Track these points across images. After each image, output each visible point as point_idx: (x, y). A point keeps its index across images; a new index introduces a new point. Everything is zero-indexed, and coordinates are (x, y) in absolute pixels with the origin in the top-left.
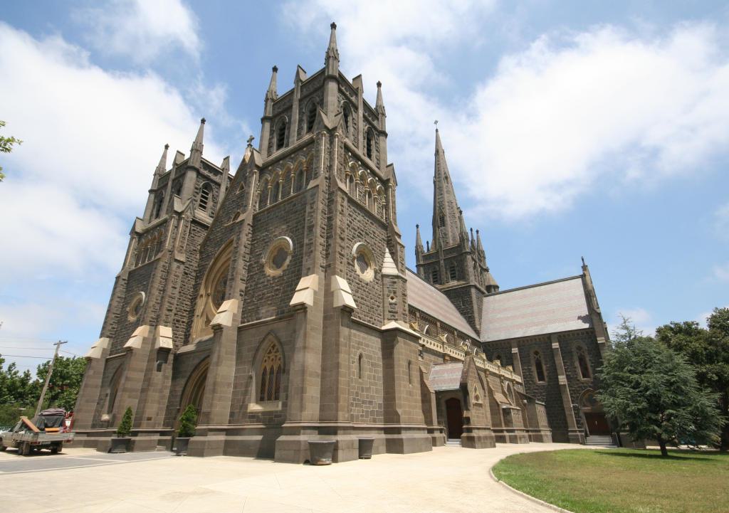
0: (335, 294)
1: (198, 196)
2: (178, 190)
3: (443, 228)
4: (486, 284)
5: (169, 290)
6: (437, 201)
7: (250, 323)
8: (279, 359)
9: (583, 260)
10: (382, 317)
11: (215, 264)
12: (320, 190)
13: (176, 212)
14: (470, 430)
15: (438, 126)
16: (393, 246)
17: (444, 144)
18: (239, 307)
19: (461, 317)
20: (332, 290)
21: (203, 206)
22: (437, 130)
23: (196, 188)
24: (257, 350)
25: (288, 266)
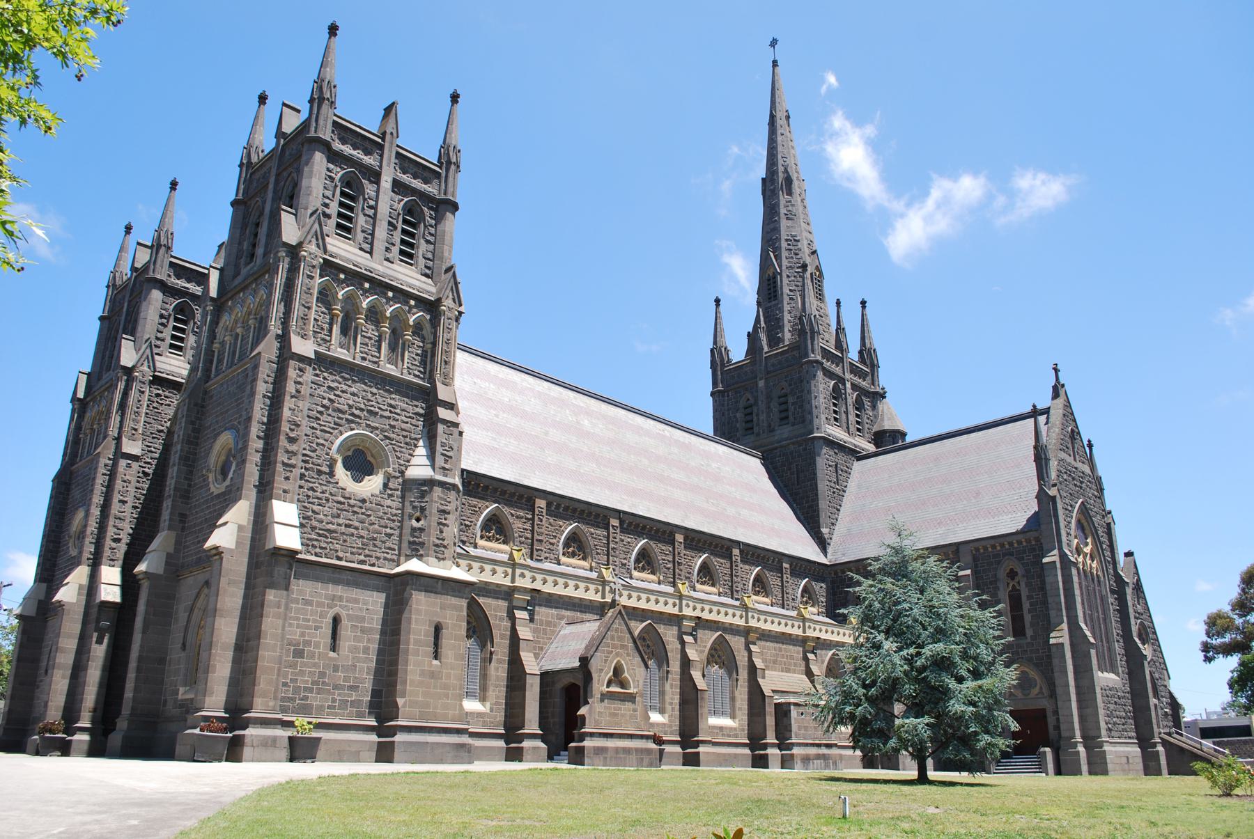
1: (165, 330)
2: (291, 197)
4: (876, 428)
5: (115, 507)
9: (1056, 370)
10: (396, 552)
12: (263, 362)
13: (124, 368)
14: (582, 737)
15: (780, 53)
17: (787, 101)
21: (344, 229)
22: (775, 63)
23: (162, 316)
24: (192, 610)
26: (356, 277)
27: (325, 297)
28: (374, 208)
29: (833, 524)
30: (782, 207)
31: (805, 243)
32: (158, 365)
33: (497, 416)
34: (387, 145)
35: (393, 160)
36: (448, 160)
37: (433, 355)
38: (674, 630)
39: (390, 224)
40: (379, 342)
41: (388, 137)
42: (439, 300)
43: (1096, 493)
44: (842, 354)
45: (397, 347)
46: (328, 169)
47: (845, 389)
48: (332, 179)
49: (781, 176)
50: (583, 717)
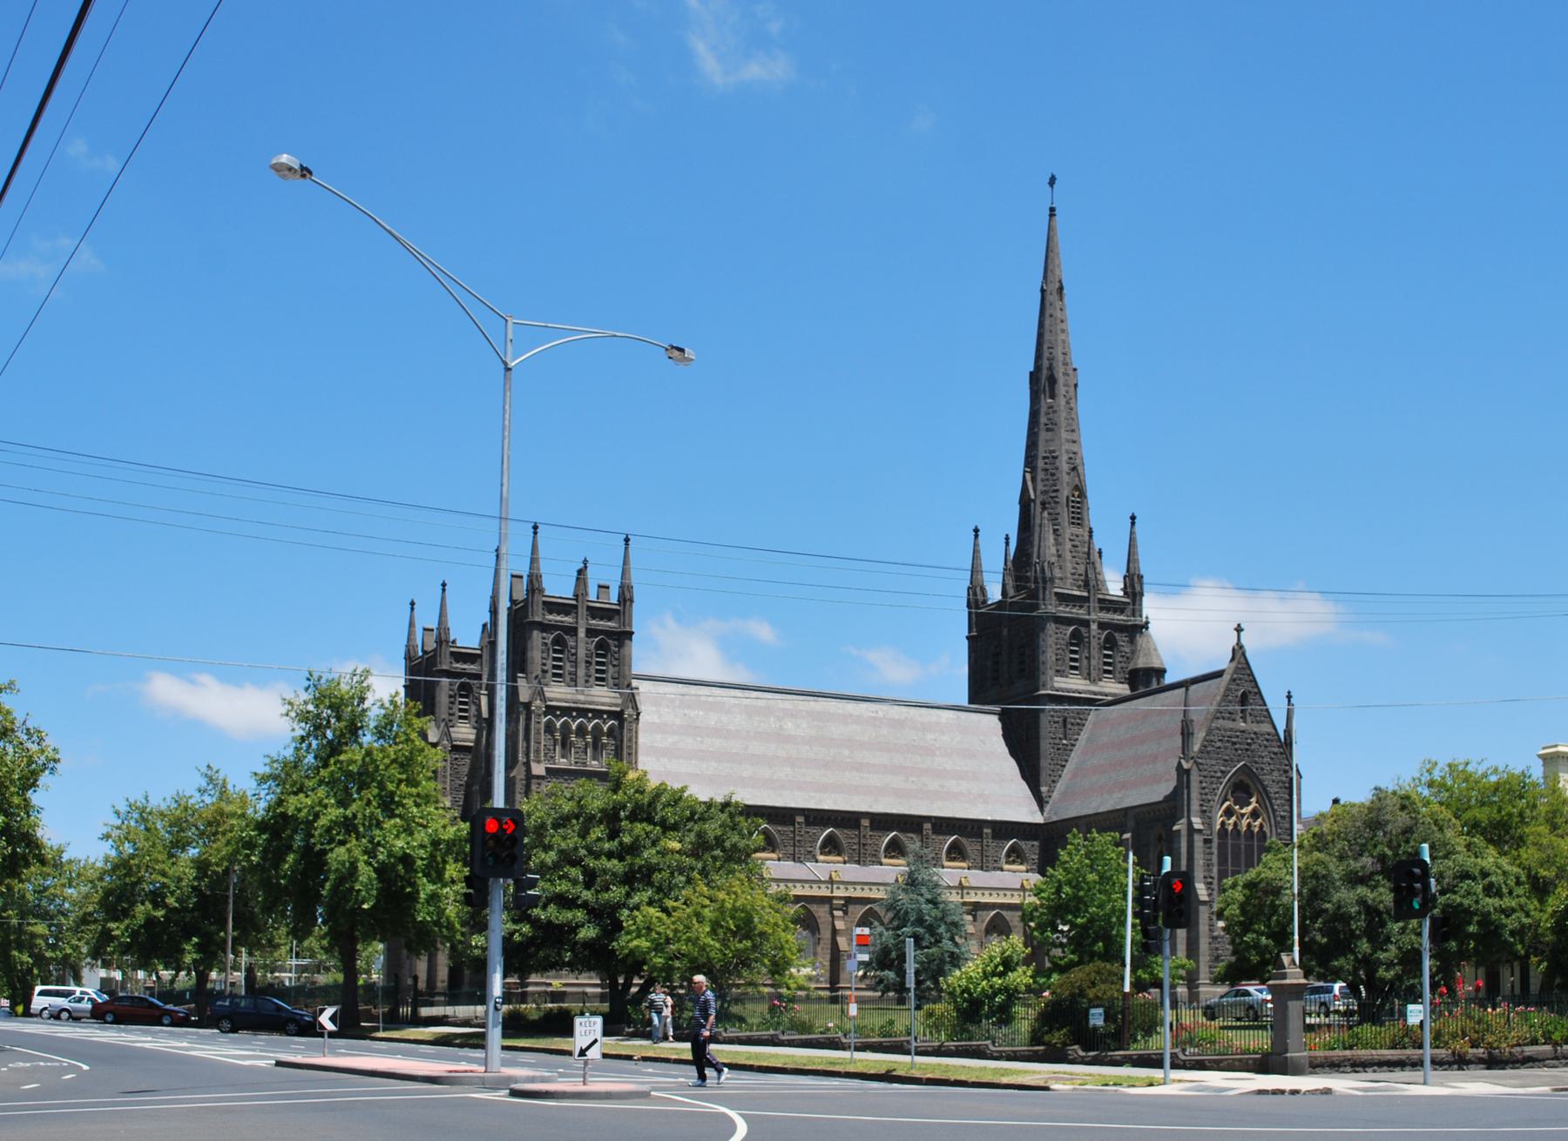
4: (1131, 666)
12: (517, 781)
17: (1068, 272)
23: (450, 696)
26: (566, 711)
27: (549, 728)
28: (575, 654)
29: (1054, 782)
30: (1042, 414)
31: (1065, 458)
32: (453, 735)
33: (702, 742)
34: (580, 605)
35: (585, 613)
36: (626, 597)
37: (622, 749)
38: (827, 907)
39: (587, 662)
40: (586, 749)
41: (580, 598)
42: (621, 713)
43: (1276, 750)
44: (1089, 592)
45: (597, 746)
46: (544, 638)
47: (1089, 632)
48: (546, 644)
49: (1045, 372)
50: (1026, 948)
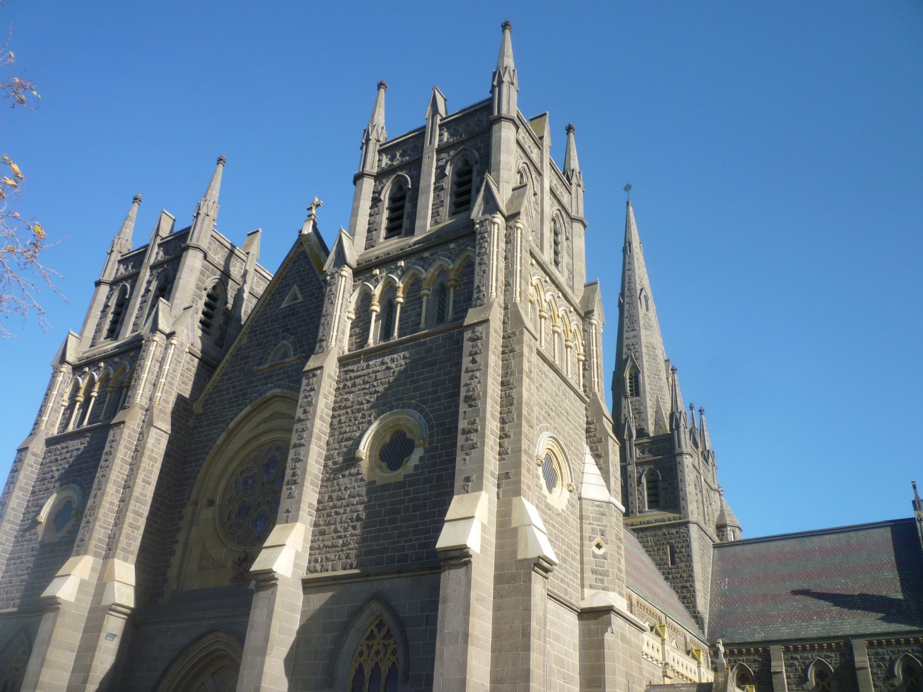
0: (520, 532)
3: (635, 398)
6: (625, 342)
7: (331, 574)
8: (394, 652)
9: (914, 487)
11: (227, 441)
16: (600, 441)
18: (305, 541)
19: (666, 586)
20: (513, 525)
25: (416, 467)
